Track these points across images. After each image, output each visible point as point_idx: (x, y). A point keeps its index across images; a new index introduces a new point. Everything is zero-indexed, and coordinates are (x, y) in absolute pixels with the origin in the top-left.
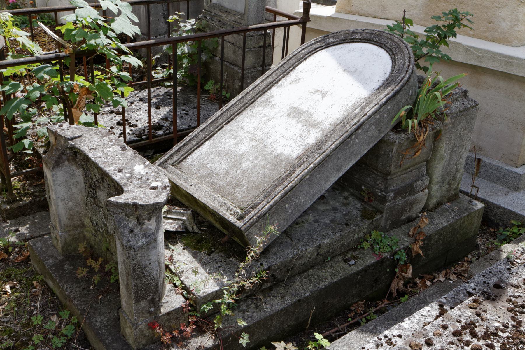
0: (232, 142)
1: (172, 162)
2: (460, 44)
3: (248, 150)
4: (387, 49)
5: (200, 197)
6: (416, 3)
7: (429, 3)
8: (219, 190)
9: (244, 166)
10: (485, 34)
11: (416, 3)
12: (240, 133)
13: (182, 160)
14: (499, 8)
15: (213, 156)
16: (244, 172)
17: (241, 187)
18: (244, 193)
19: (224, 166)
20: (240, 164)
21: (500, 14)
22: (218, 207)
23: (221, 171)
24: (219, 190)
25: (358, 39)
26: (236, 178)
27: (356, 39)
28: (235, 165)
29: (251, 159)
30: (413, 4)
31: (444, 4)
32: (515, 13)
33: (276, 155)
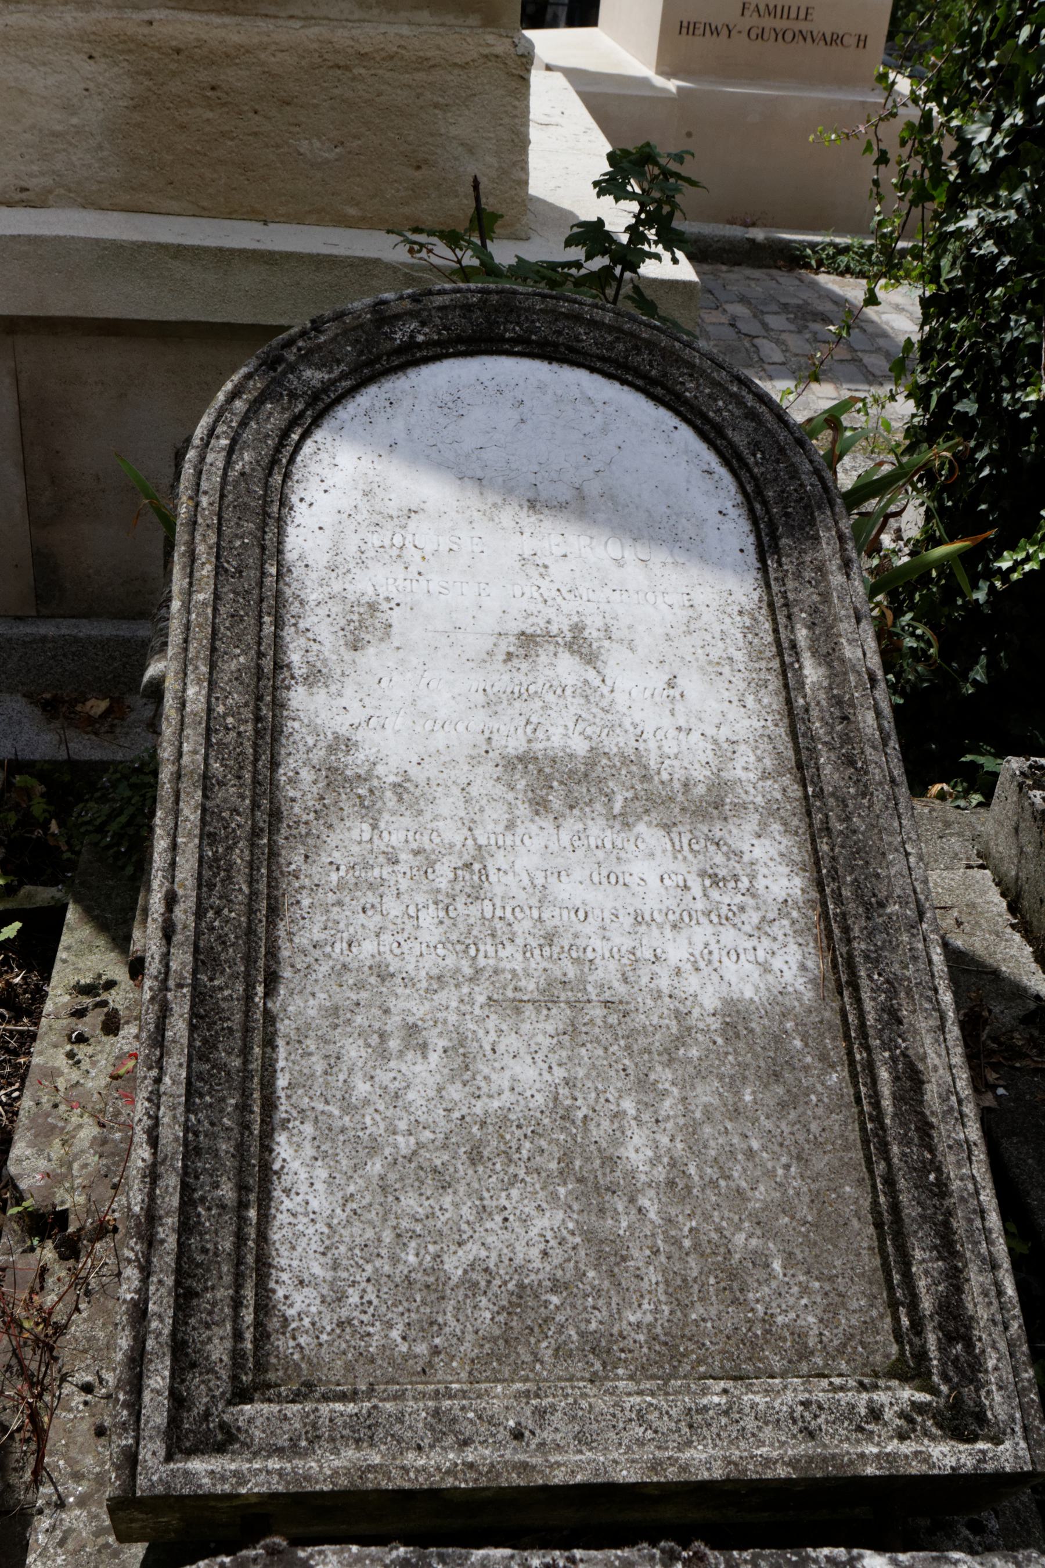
0: (423, 1073)
1: (222, 1387)
2: (377, 261)
3: (559, 1073)
4: (606, 367)
5: (655, 1466)
6: (74, 121)
7: (137, 117)
8: (669, 1357)
9: (637, 1152)
10: (406, 210)
11: (74, 121)
12: (409, 1005)
13: (262, 1336)
14: (445, 108)
15: (410, 1202)
16: (676, 1186)
17: (760, 1274)
18: (805, 1290)
19: (541, 1223)
20: (610, 1161)
21: (454, 131)
22: (802, 1448)
23: (558, 1255)
24: (669, 1357)
25: (427, 344)
26: (677, 1242)
27: (419, 346)
28: (593, 1180)
29: (628, 1105)
30: (59, 128)
31: (210, 115)
32: (507, 120)
33: (715, 1024)
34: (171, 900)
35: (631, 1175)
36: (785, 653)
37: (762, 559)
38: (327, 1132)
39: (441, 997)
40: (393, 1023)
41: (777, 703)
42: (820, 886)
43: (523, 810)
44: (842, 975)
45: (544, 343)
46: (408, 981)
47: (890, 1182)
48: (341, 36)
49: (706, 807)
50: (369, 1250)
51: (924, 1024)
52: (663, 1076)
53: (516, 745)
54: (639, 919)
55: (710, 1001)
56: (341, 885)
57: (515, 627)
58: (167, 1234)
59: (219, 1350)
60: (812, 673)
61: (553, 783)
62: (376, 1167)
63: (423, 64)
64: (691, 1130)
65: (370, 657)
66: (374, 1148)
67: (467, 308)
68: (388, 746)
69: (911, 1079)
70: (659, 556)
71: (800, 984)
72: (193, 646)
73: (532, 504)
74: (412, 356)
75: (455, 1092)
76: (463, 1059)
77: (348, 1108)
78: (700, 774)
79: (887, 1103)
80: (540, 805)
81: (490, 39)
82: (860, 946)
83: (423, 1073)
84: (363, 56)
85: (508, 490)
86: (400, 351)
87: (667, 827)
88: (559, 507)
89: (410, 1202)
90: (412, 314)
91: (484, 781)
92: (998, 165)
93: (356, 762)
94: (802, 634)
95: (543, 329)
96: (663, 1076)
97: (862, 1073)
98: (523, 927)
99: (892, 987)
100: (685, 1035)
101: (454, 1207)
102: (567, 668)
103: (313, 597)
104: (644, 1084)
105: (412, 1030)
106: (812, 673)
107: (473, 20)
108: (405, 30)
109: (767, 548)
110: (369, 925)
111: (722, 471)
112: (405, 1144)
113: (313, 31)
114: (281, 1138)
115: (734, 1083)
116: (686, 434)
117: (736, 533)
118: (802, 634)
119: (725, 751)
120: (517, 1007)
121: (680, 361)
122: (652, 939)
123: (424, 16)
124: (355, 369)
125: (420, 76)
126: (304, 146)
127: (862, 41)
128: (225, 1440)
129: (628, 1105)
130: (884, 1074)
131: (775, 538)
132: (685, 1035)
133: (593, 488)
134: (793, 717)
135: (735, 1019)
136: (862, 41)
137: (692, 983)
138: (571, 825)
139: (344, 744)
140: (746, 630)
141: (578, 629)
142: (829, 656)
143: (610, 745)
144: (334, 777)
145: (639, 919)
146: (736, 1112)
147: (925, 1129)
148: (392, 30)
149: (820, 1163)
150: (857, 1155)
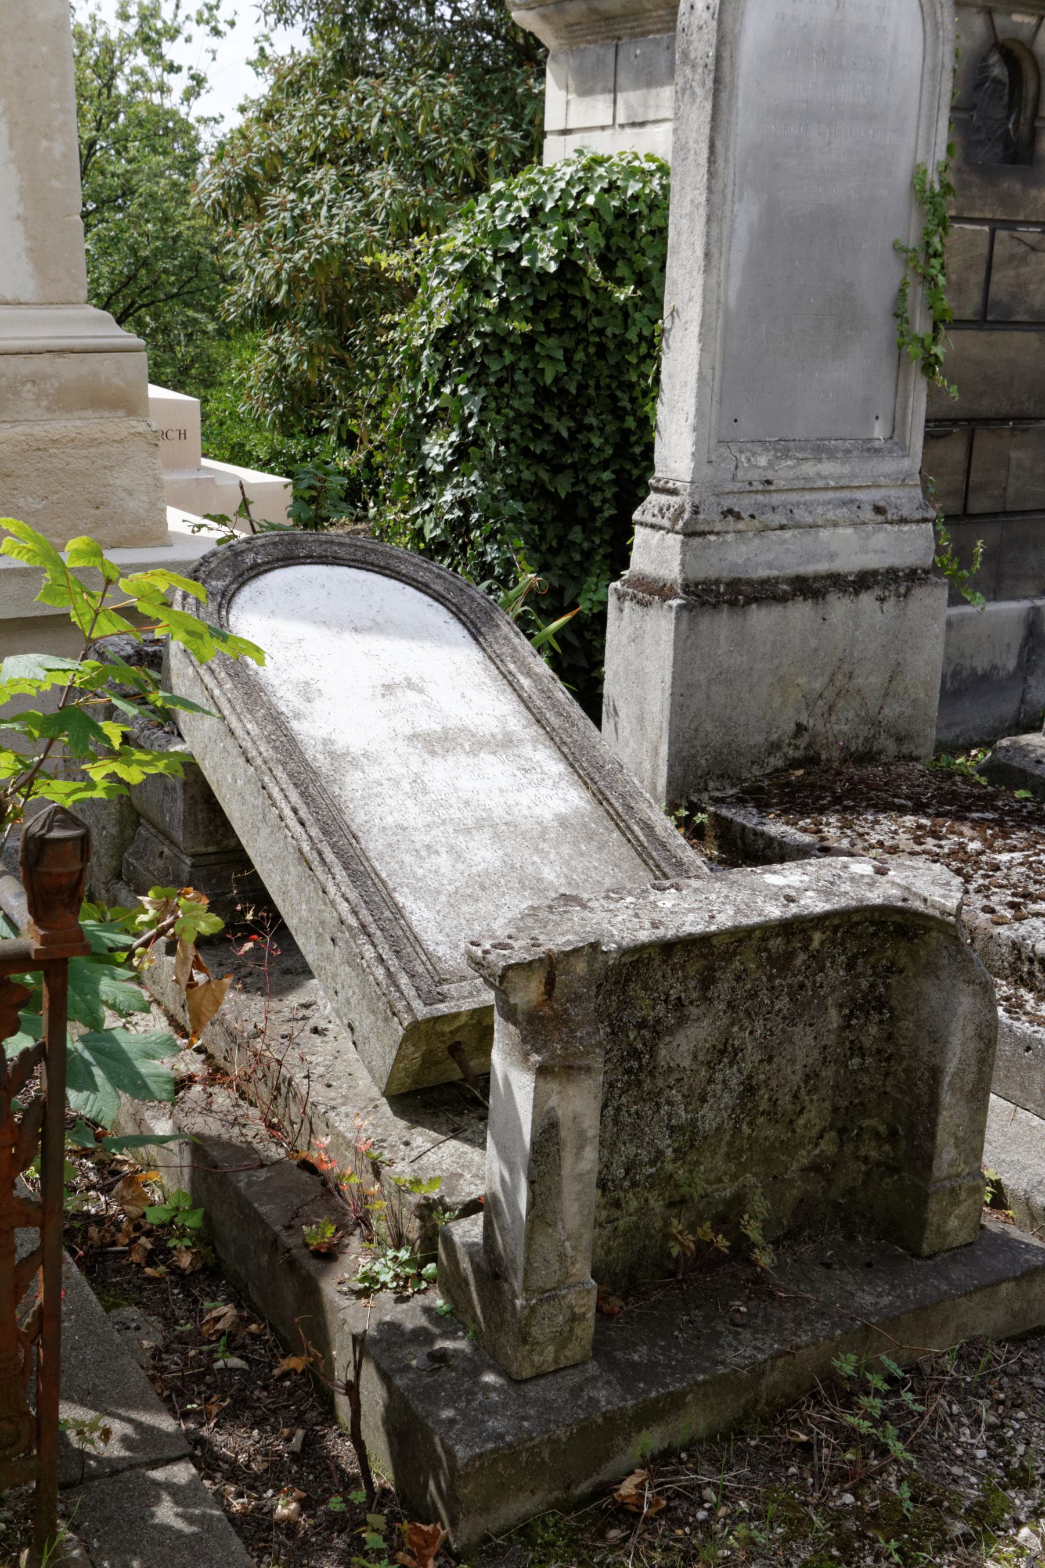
14: (110, 468)
21: (118, 482)
34: (295, 811)
35: (551, 883)
36: (507, 677)
37: (476, 639)
38: (414, 890)
39: (433, 832)
40: (418, 846)
41: (515, 697)
42: (572, 766)
43: (426, 756)
44: (600, 798)
45: (320, 557)
46: (416, 829)
47: (657, 866)
48: (38, 430)
49: (507, 743)
50: (459, 928)
51: (644, 806)
52: (546, 846)
53: (408, 731)
54: (501, 791)
55: (550, 817)
56: (363, 798)
57: (379, 683)
58: (373, 928)
59: (420, 969)
60: (525, 682)
61: (438, 743)
62: (443, 898)
63: (93, 442)
64: (567, 863)
65: (318, 704)
66: (439, 893)
67: (275, 544)
68: (350, 738)
69: (648, 828)
70: (428, 645)
71: (582, 803)
72: (238, 709)
73: (356, 630)
74: (257, 571)
75: (460, 866)
76: (457, 855)
77: (418, 880)
78: (496, 731)
79: (642, 838)
80: (433, 753)
81: (134, 423)
82: (601, 784)
83: (443, 862)
84: (54, 441)
85: (341, 627)
86: (251, 568)
87: (494, 753)
88: (370, 629)
89: (464, 908)
90: (250, 550)
91: (402, 746)
92: (449, 466)
93: (339, 747)
94: (512, 667)
95: (317, 550)
96: (546, 846)
97: (624, 830)
98: (453, 801)
99: (622, 796)
100: (545, 831)
101: (484, 907)
102: (412, 696)
103: (276, 682)
104: (537, 850)
105: (428, 847)
106: (525, 682)
107: (121, 413)
108: (78, 423)
109: (476, 635)
110: (384, 808)
111: (436, 604)
112: (451, 889)
113: (20, 429)
114: (396, 895)
115: (575, 843)
116: (409, 590)
117: (457, 630)
118: (512, 667)
119: (502, 720)
120: (468, 831)
121: (391, 556)
122: (511, 798)
123: (89, 413)
124: (235, 579)
125: (92, 450)
126: (22, 502)
127: (182, 435)
128: (443, 998)
129: (536, 859)
130: (636, 828)
131: (478, 629)
132: (545, 831)
133: (380, 619)
134: (525, 702)
135: (563, 822)
136: (182, 435)
137: (537, 811)
138: (451, 759)
139: (326, 742)
140: (485, 670)
141: (408, 680)
142: (529, 673)
143: (450, 724)
144: (333, 755)
145: (501, 791)
146: (582, 854)
147: (663, 845)
148: (69, 424)
149: (626, 866)
150: (639, 861)
